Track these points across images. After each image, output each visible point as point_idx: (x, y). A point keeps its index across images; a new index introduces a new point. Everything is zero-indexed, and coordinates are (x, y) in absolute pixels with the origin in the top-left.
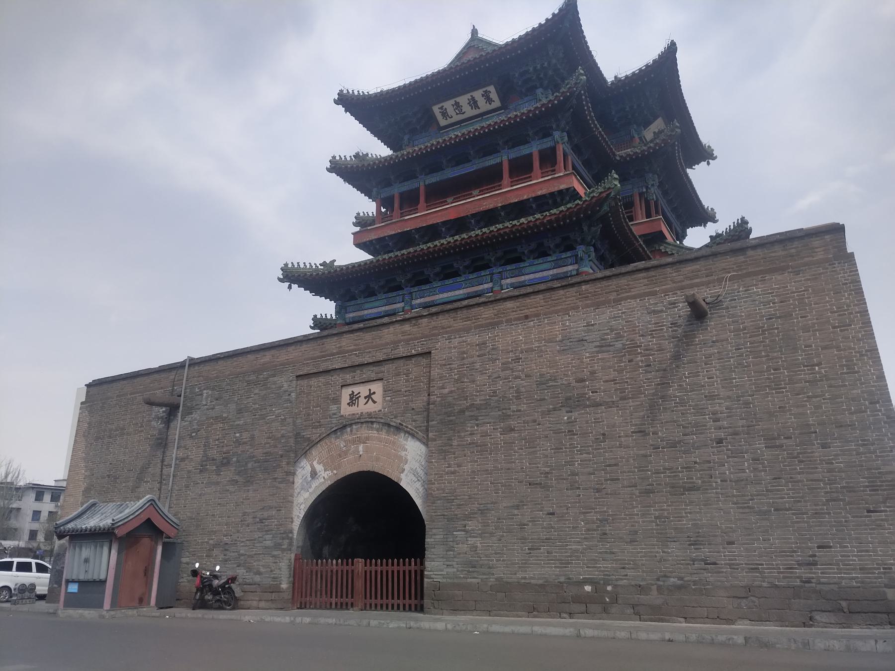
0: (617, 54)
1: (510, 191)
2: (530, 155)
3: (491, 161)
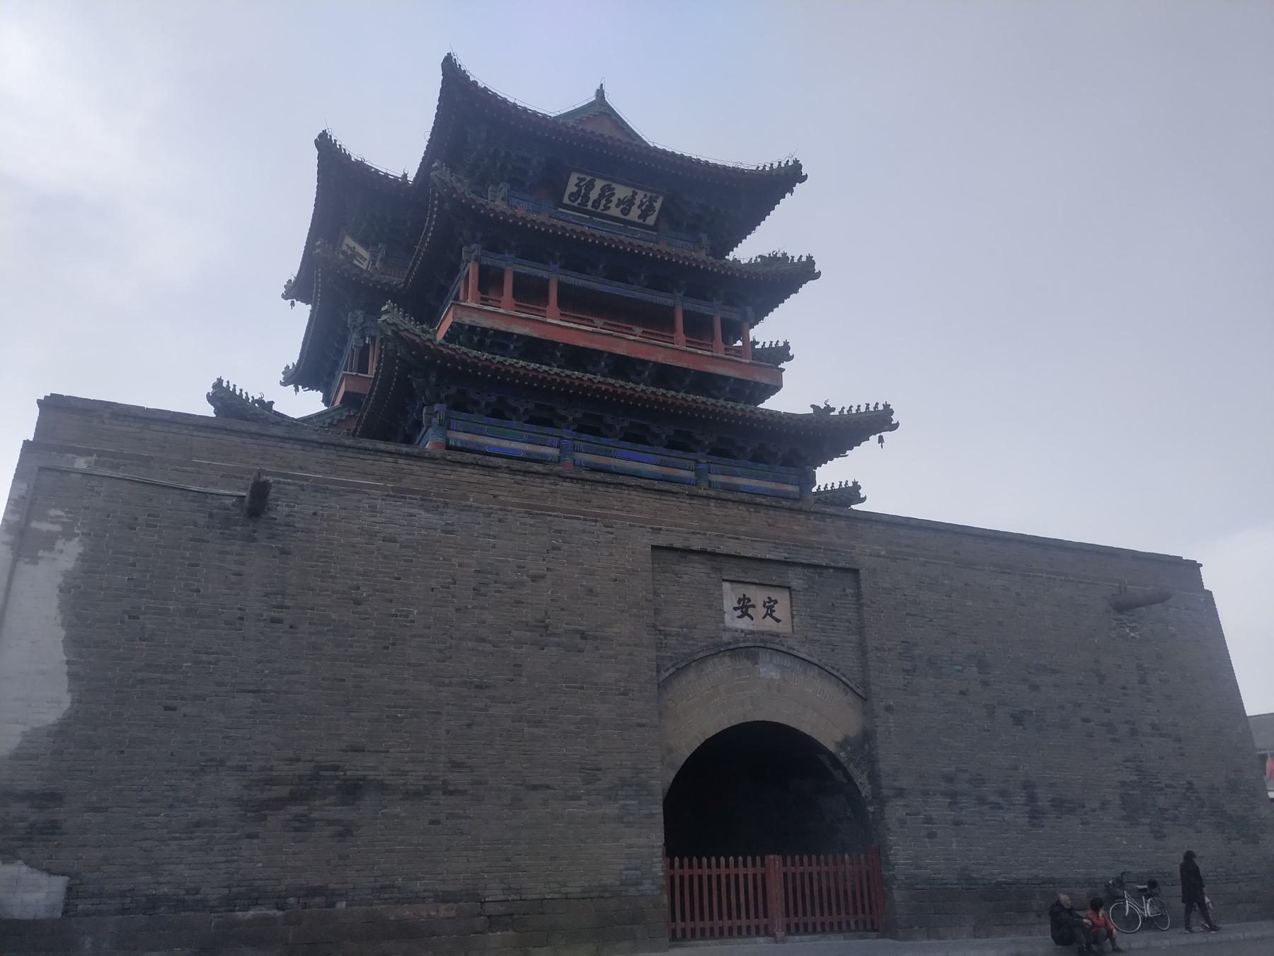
0: (397, 145)
1: (629, 343)
2: (671, 309)
3: (660, 299)
